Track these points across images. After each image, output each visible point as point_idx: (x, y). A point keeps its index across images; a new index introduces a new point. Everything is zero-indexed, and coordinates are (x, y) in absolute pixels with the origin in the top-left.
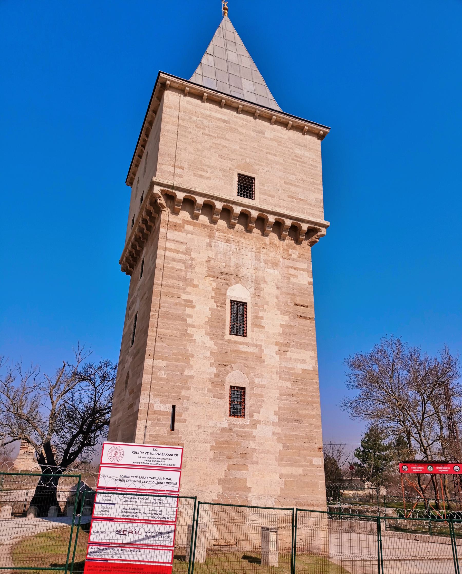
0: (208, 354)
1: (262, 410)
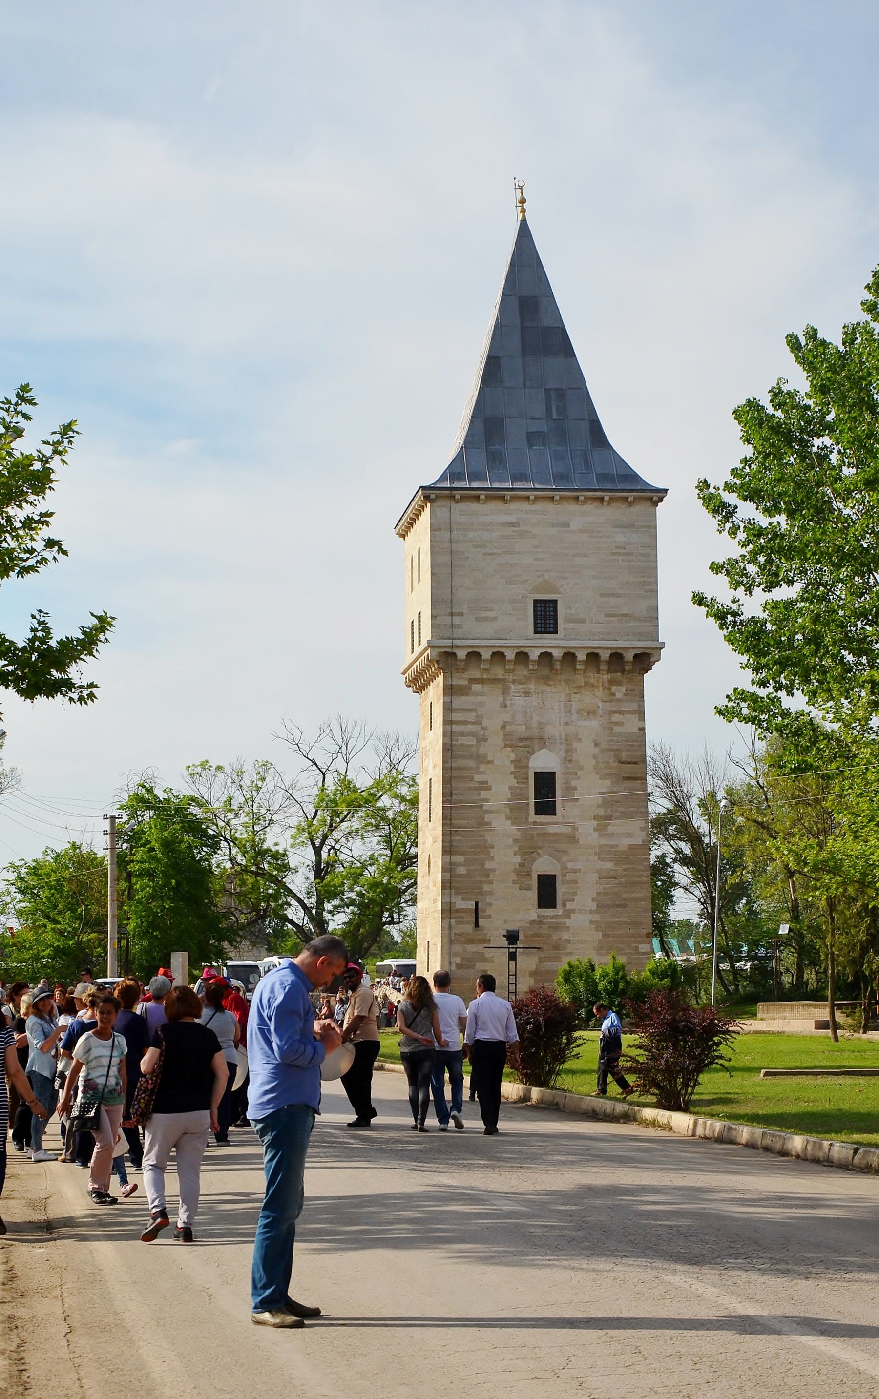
0: (511, 841)
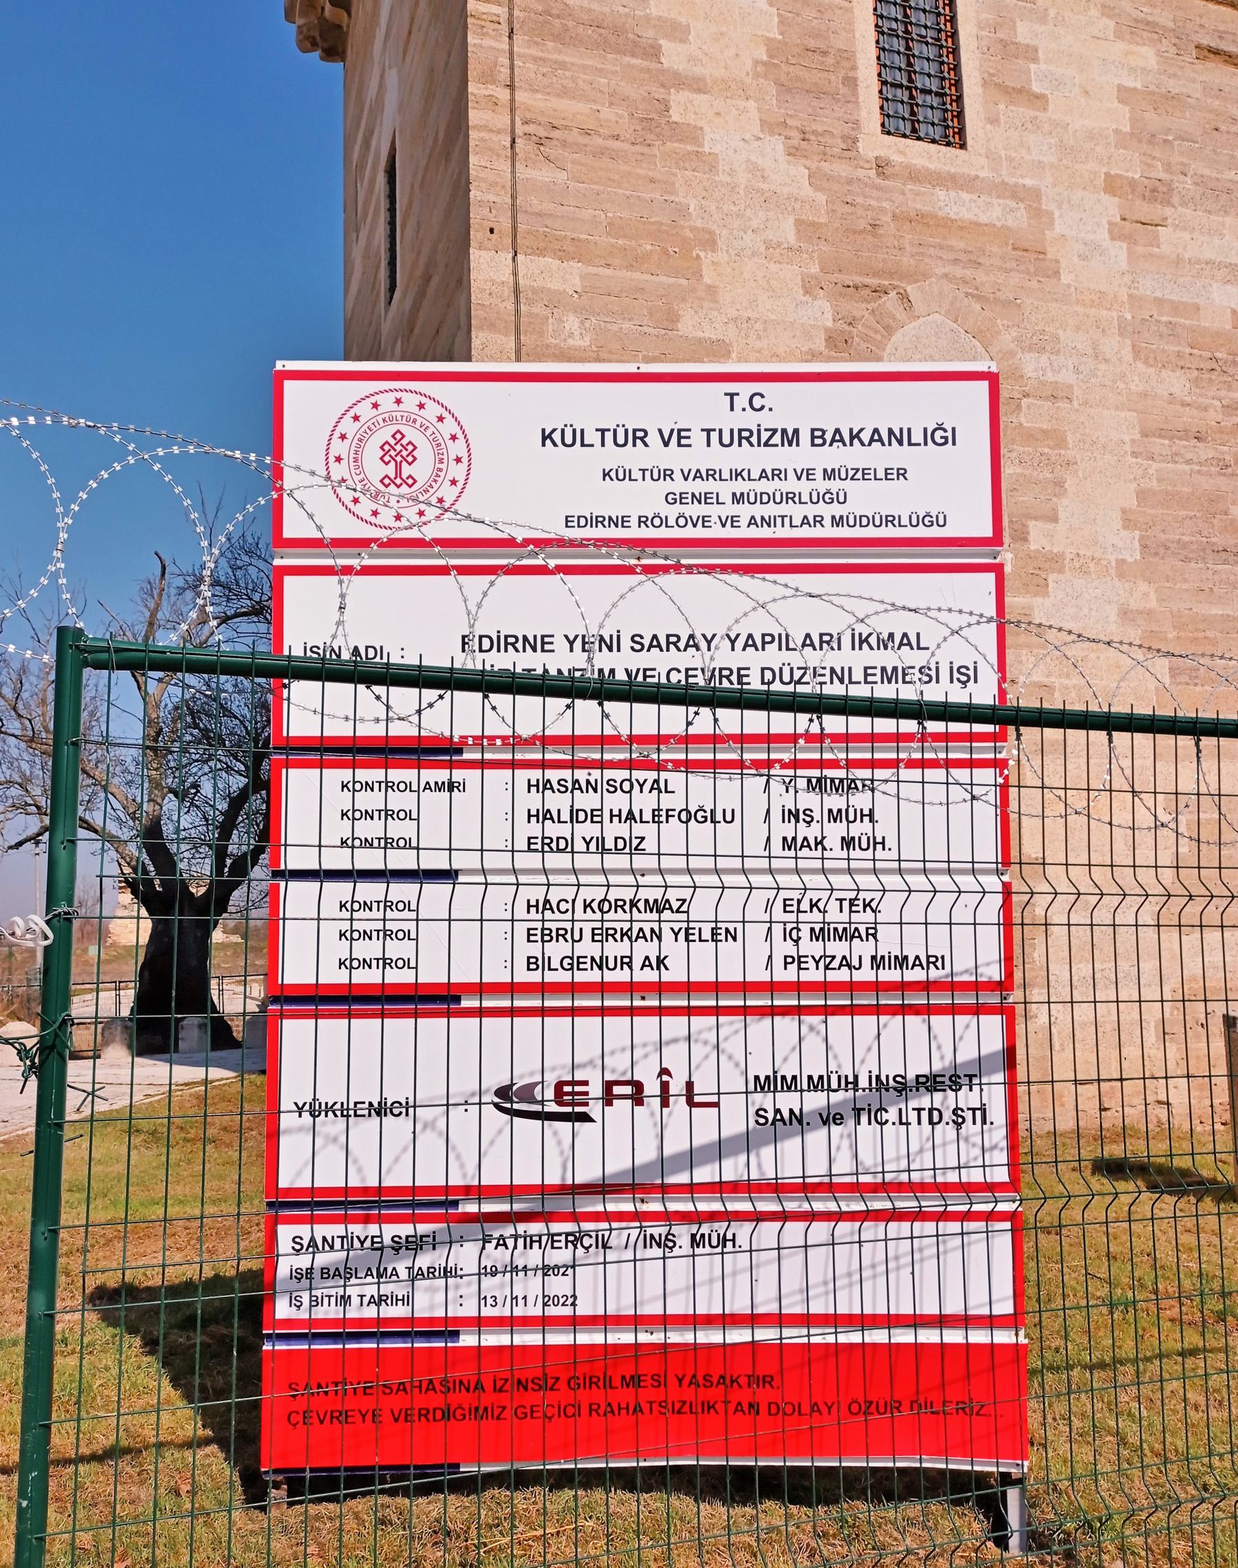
0: (787, 231)
1: (1067, 508)
